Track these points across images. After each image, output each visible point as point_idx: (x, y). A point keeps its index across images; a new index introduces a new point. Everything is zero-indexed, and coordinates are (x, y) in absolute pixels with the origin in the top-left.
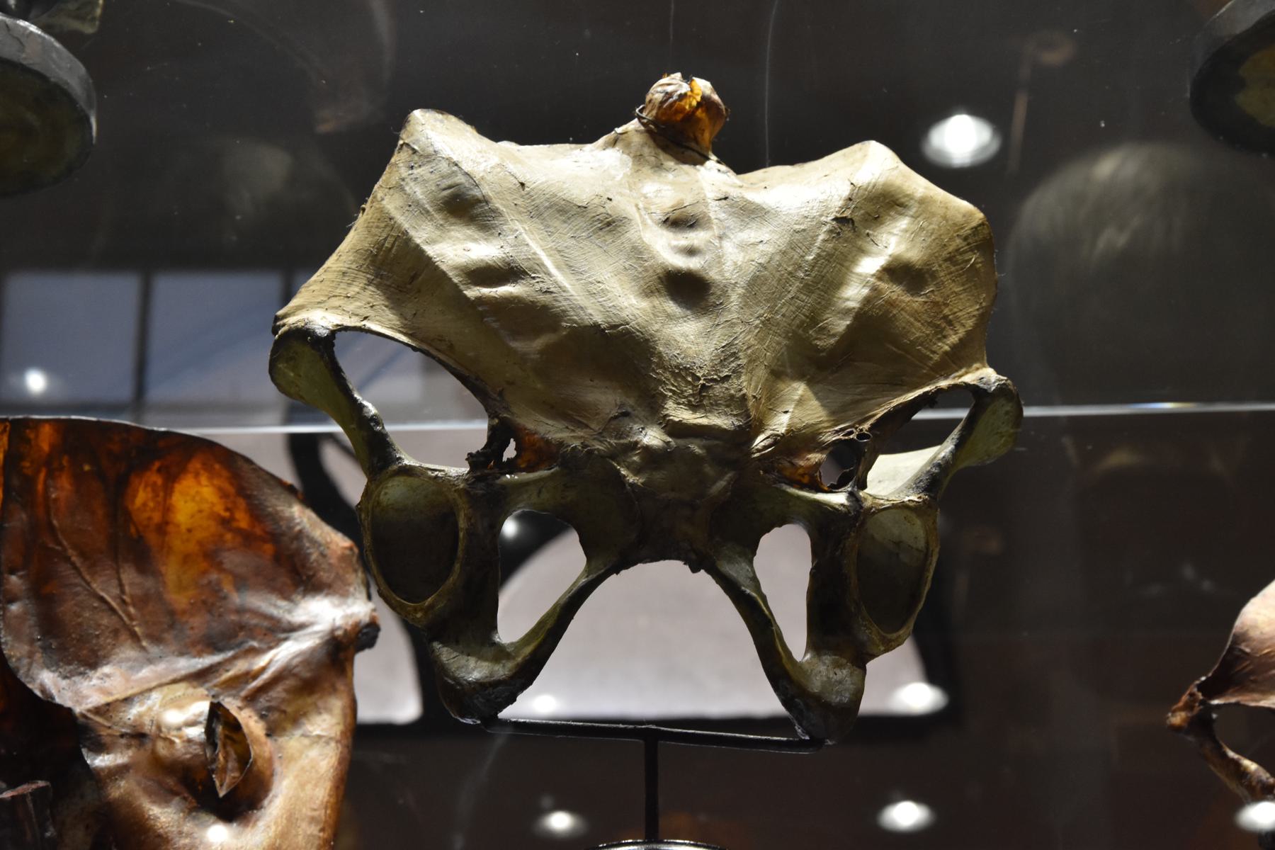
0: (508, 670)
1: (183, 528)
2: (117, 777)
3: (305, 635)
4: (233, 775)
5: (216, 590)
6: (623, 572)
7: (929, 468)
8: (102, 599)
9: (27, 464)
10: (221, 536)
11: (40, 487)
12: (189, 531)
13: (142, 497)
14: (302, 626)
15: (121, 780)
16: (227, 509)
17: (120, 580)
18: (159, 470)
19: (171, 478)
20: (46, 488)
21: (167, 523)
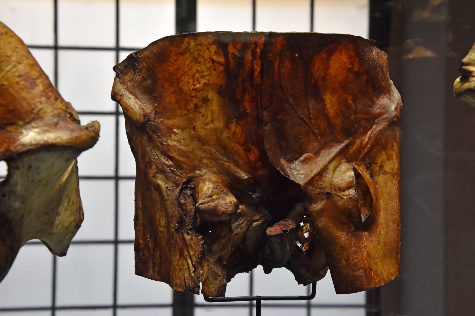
0: (195, 54)
1: (333, 76)
2: (320, 216)
3: (381, 120)
4: (361, 202)
5: (123, 81)
6: (243, 273)
7: (337, 185)
8: (302, 119)
9: (271, 55)
10: (348, 76)
11: (276, 66)
12: (335, 77)
13: (318, 64)
14: (379, 115)
15: (322, 218)
16: (351, 64)
17: (308, 107)
18: (326, 52)
19: (330, 54)
20: (279, 67)
21: (326, 75)
